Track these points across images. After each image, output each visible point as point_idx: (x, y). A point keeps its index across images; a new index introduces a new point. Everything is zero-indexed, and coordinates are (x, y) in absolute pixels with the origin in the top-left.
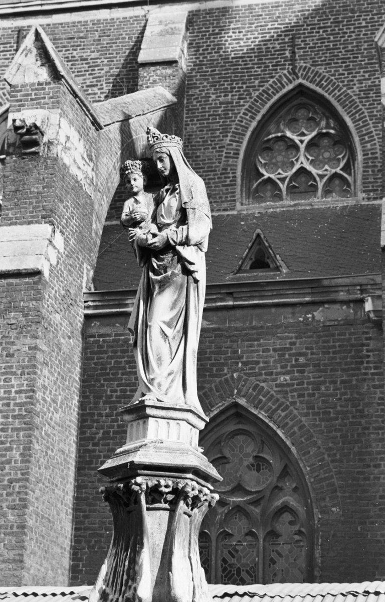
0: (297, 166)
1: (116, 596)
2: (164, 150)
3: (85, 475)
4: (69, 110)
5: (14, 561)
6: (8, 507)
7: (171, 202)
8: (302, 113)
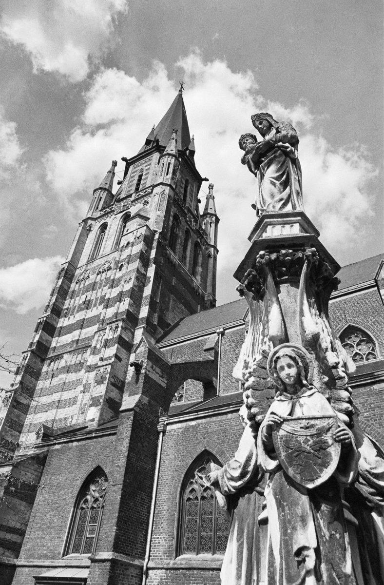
0: (354, 352)
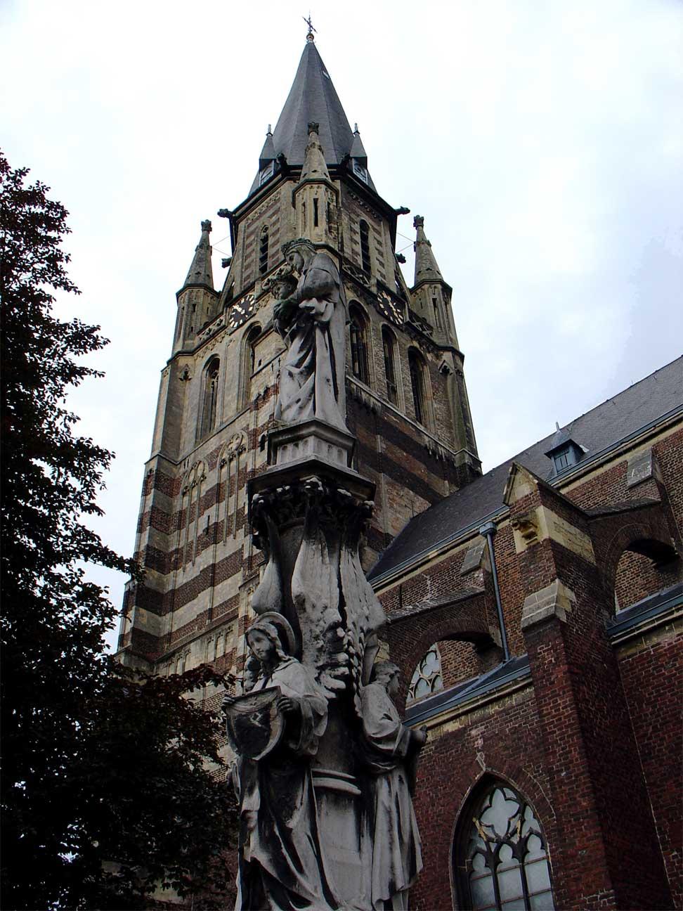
3: (649, 764)
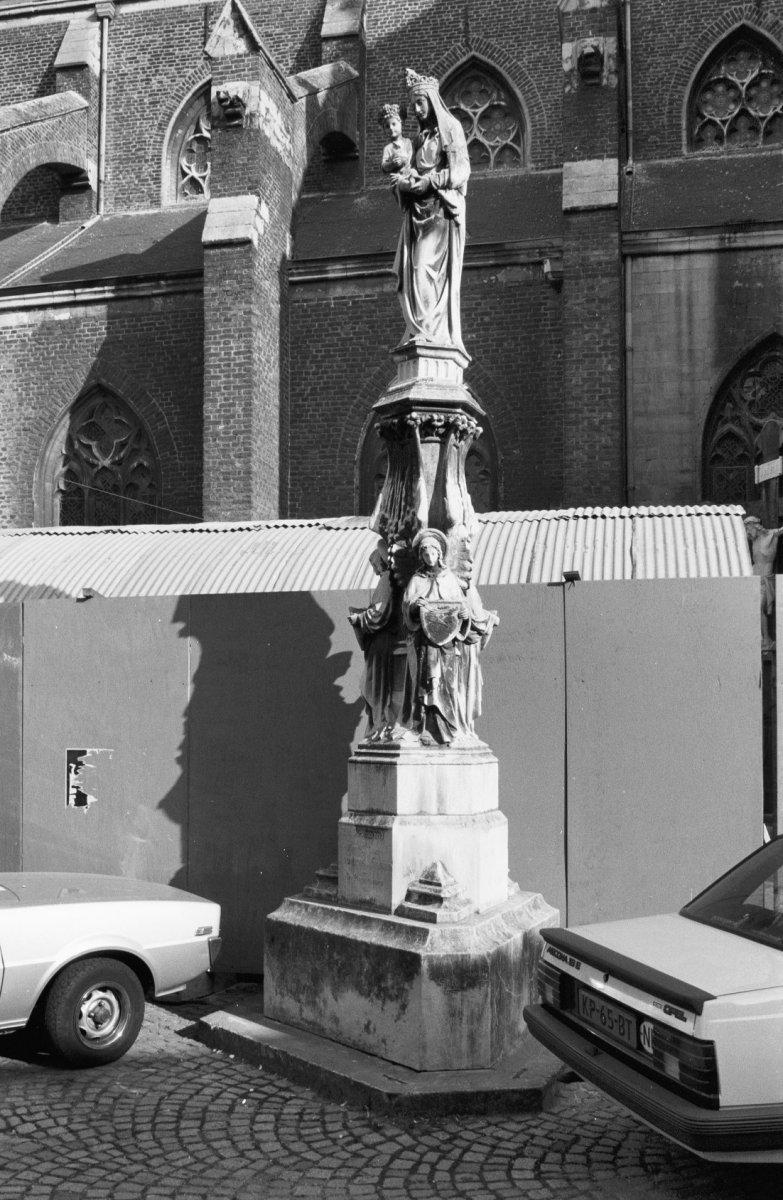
1: (396, 520)
2: (423, 92)
4: (267, 82)
5: (243, 502)
6: (235, 456)
7: (431, 146)
8: (474, 86)
